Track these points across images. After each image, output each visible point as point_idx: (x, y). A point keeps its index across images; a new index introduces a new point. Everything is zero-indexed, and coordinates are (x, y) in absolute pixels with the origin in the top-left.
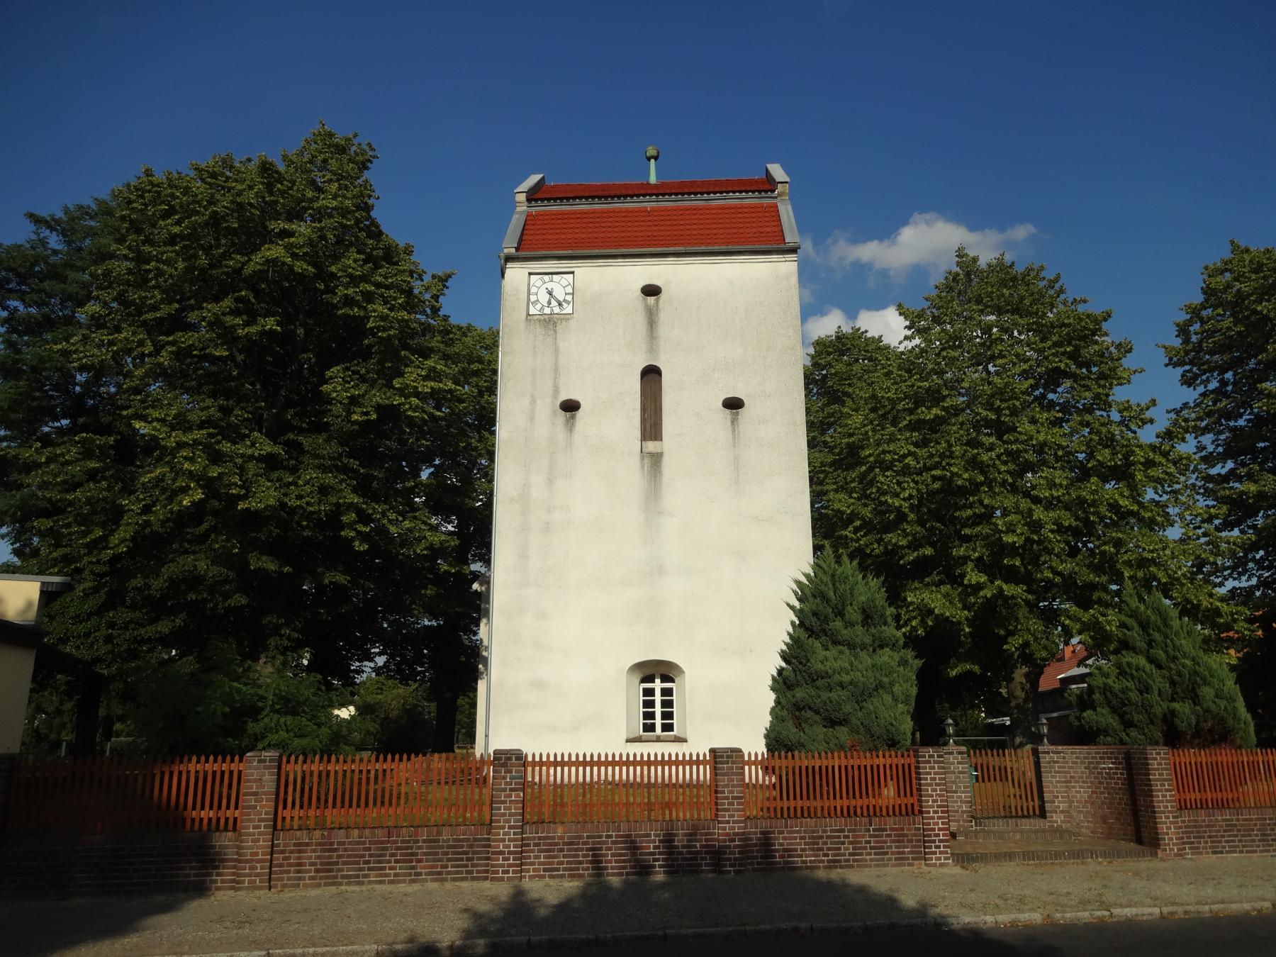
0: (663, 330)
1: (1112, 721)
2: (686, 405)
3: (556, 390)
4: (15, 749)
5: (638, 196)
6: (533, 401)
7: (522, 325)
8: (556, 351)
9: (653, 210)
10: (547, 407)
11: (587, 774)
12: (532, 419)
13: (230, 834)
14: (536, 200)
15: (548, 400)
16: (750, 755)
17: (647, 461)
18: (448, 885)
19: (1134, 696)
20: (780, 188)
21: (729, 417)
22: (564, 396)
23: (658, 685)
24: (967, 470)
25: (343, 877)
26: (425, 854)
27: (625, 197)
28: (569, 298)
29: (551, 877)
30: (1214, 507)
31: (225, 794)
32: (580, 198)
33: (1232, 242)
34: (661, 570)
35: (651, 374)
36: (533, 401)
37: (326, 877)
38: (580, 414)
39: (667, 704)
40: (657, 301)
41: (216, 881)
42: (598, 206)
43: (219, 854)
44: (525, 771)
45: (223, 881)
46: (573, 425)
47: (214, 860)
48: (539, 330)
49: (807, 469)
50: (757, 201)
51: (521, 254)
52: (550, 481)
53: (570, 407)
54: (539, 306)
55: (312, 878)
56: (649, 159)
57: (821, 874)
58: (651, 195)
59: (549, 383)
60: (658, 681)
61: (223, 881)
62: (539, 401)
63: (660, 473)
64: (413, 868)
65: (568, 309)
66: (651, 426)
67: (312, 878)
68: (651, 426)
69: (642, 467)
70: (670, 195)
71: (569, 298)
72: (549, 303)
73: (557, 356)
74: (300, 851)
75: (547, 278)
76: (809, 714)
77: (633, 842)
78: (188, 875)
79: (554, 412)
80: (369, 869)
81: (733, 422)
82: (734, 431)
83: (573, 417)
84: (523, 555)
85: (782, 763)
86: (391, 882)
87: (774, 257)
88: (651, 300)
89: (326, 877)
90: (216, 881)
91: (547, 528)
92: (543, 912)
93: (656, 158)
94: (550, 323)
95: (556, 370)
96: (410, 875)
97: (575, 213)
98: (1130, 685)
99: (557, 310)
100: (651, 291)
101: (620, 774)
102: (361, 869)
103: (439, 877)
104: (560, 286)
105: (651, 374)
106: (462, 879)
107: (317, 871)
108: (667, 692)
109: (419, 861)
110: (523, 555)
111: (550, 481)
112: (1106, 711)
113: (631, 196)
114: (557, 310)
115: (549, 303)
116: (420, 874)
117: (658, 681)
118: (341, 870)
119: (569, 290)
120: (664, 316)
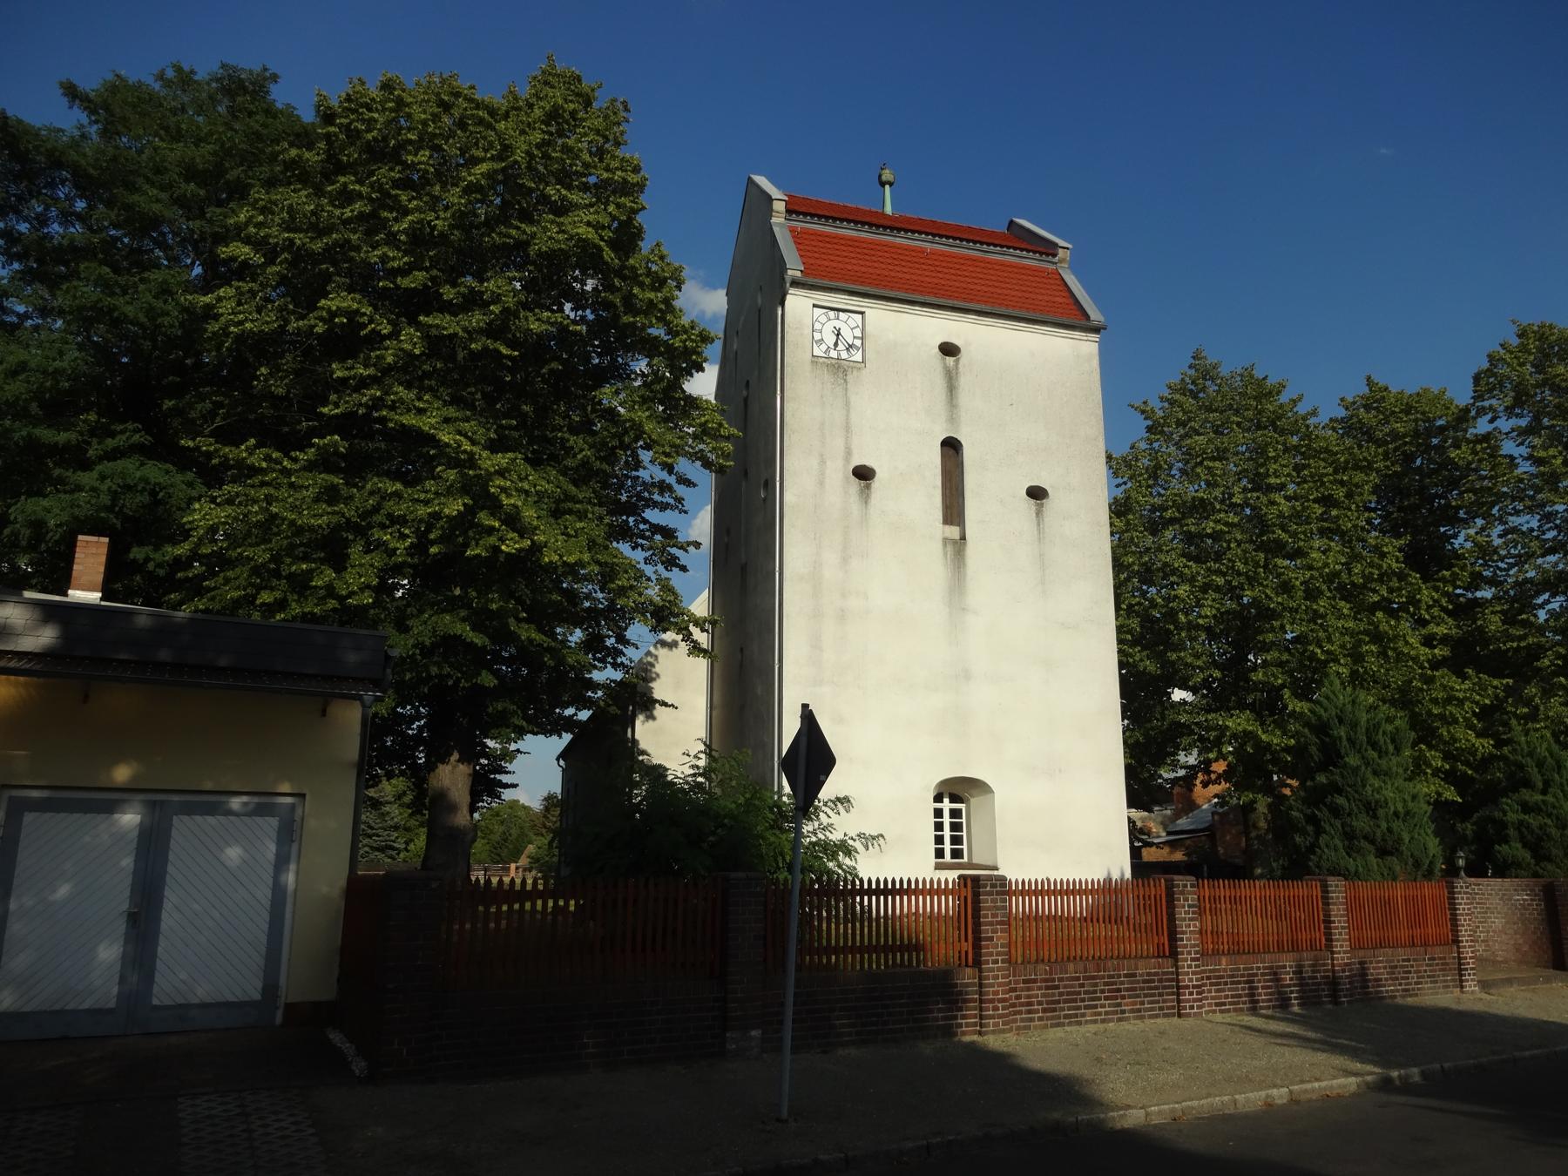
0: (964, 398)
1: (1526, 855)
3: (848, 453)
5: (913, 232)
6: (823, 462)
7: (808, 367)
8: (847, 404)
9: (933, 253)
10: (838, 474)
12: (821, 483)
13: (968, 970)
14: (798, 213)
15: (840, 463)
16: (870, 881)
17: (949, 548)
18: (1148, 1021)
19: (1553, 831)
22: (856, 462)
23: (946, 805)
24: (1277, 594)
25: (1066, 1017)
26: (1127, 990)
27: (899, 230)
28: (858, 343)
29: (1222, 1012)
32: (849, 221)
33: (1369, 378)
34: (967, 675)
35: (951, 447)
36: (823, 462)
38: (876, 483)
39: (956, 827)
40: (957, 362)
41: (960, 1025)
42: (864, 234)
43: (960, 993)
45: (967, 1025)
46: (868, 496)
47: (957, 1001)
48: (827, 377)
50: (863, 235)
51: (810, 280)
52: (845, 560)
53: (864, 474)
54: (824, 347)
55: (1040, 1019)
56: (883, 184)
57: (1399, 1001)
58: (927, 234)
59: (839, 443)
60: (946, 800)
61: (967, 1025)
64: (1119, 1005)
65: (858, 357)
66: (953, 510)
67: (1040, 1019)
68: (953, 510)
70: (948, 237)
71: (858, 343)
72: (836, 344)
74: (1029, 989)
75: (832, 314)
76: (1364, 844)
77: (1275, 974)
78: (937, 1019)
79: (847, 478)
80: (1086, 1007)
83: (868, 487)
84: (816, 644)
86: (1103, 1021)
87: (1077, 334)
88: (950, 360)
89: (1052, 1018)
90: (960, 1025)
91: (842, 616)
93: (891, 184)
94: (839, 369)
95: (847, 428)
96: (1116, 1013)
97: (836, 237)
98: (1549, 822)
99: (844, 355)
100: (948, 350)
102: (1079, 1008)
103: (1139, 1014)
104: (849, 326)
105: (951, 447)
106: (1157, 1016)
107: (1044, 1011)
108: (955, 813)
109: (1123, 997)
110: (816, 644)
111: (845, 560)
112: (1519, 845)
113: (906, 231)
114: (844, 355)
115: (836, 344)
116: (1123, 1012)
117: (946, 800)
118: (1063, 1009)
119: (858, 333)
120: (964, 381)
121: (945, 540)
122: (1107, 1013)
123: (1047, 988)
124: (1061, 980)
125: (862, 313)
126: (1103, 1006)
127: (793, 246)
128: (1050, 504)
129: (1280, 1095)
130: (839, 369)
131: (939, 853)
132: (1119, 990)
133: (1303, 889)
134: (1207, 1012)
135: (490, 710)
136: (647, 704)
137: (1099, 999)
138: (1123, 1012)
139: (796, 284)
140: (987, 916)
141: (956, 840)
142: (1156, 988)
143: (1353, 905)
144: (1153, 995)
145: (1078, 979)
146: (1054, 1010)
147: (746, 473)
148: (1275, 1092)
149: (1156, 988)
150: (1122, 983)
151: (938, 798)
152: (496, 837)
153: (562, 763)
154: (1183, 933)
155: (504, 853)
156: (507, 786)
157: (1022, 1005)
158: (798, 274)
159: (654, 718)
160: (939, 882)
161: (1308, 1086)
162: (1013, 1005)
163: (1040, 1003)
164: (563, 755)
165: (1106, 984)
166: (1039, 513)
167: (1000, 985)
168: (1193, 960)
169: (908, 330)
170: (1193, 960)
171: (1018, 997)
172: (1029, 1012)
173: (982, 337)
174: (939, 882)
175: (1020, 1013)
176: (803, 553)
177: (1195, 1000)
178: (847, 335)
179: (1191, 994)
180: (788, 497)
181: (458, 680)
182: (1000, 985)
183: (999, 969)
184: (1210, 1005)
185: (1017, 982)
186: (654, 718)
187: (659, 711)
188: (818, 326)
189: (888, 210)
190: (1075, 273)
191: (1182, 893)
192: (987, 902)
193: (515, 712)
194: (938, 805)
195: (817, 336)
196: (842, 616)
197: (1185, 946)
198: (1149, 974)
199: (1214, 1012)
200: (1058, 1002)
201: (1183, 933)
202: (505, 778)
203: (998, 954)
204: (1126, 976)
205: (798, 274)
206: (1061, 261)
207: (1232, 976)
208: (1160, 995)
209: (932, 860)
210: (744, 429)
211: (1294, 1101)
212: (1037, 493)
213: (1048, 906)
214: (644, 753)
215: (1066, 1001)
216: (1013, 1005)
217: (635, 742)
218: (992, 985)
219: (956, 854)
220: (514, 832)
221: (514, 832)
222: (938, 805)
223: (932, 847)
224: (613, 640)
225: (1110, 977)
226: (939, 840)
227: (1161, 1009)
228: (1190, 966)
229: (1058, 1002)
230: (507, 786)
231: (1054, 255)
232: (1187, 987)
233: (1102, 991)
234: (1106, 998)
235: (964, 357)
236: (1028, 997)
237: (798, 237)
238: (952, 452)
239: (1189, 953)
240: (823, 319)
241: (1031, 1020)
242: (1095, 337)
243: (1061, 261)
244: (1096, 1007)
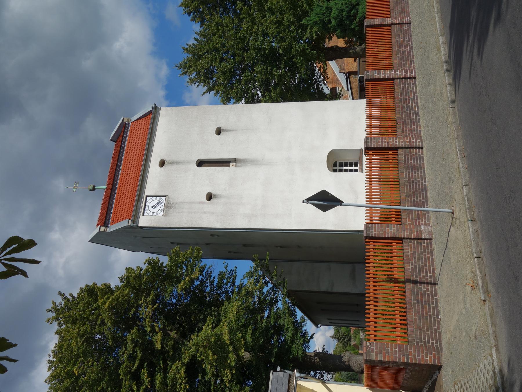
2: (218, 150)
3: (202, 203)
4: (361, 228)
6: (205, 212)
11: (375, 184)
12: (213, 213)
17: (239, 165)
20: (125, 121)
21: (224, 133)
22: (204, 199)
23: (338, 168)
29: (414, 63)
35: (201, 163)
36: (205, 212)
37: (417, 122)
38: (213, 192)
44: (374, 137)
53: (210, 197)
64: (412, 99)
73: (185, 202)
74: (406, 131)
75: (147, 208)
80: (413, 110)
81: (227, 131)
83: (215, 195)
85: (369, 94)
89: (417, 122)
94: (168, 206)
95: (191, 203)
100: (162, 164)
101: (375, 176)
102: (413, 113)
104: (151, 202)
105: (201, 163)
107: (414, 125)
109: (409, 97)
116: (414, 97)
118: (413, 119)
120: (174, 158)
122: (415, 103)
123: (406, 124)
124: (402, 119)
125: (147, 196)
126: (412, 104)
127: (119, 223)
128: (223, 126)
129: (441, 39)
131: (356, 171)
132: (406, 99)
133: (369, 34)
134: (414, 68)
137: (409, 106)
138: (414, 97)
140: (379, 145)
141: (351, 165)
142: (405, 86)
143: (375, 16)
144: (408, 87)
145: (402, 113)
146: (414, 122)
148: (441, 41)
149: (405, 86)
150: (404, 98)
151: (335, 171)
153: (319, 325)
154: (385, 76)
157: (412, 133)
158: (130, 221)
160: (366, 170)
161: (439, 29)
162: (412, 136)
163: (411, 127)
164: (316, 325)
165: (404, 103)
166: (226, 131)
167: (405, 141)
168: (395, 72)
169: (155, 179)
170: (395, 72)
171: (409, 134)
172: (414, 130)
173: (158, 151)
174: (366, 170)
175: (415, 134)
177: (410, 72)
179: (407, 73)
182: (405, 141)
183: (399, 141)
184: (411, 67)
185: (404, 135)
188: (151, 214)
189: (105, 187)
190: (133, 116)
191: (371, 76)
192: (374, 145)
194: (338, 170)
195: (155, 214)
197: (390, 75)
198: (400, 88)
199: (414, 66)
200: (411, 120)
201: (385, 76)
203: (393, 141)
204: (401, 96)
205: (130, 221)
206: (128, 121)
207: (401, 59)
208: (408, 84)
209: (358, 173)
210: (189, 244)
211: (438, 13)
212: (219, 132)
213: (376, 123)
215: (410, 117)
216: (412, 136)
218: (405, 143)
219: (356, 164)
222: (338, 170)
223: (353, 173)
225: (401, 102)
226: (351, 171)
227: (413, 84)
228: (397, 74)
229: (411, 120)
232: (405, 75)
233: (407, 105)
234: (409, 103)
235: (165, 158)
236: (409, 131)
237: (114, 222)
239: (393, 74)
240: (148, 212)
241: (417, 130)
244: (412, 107)
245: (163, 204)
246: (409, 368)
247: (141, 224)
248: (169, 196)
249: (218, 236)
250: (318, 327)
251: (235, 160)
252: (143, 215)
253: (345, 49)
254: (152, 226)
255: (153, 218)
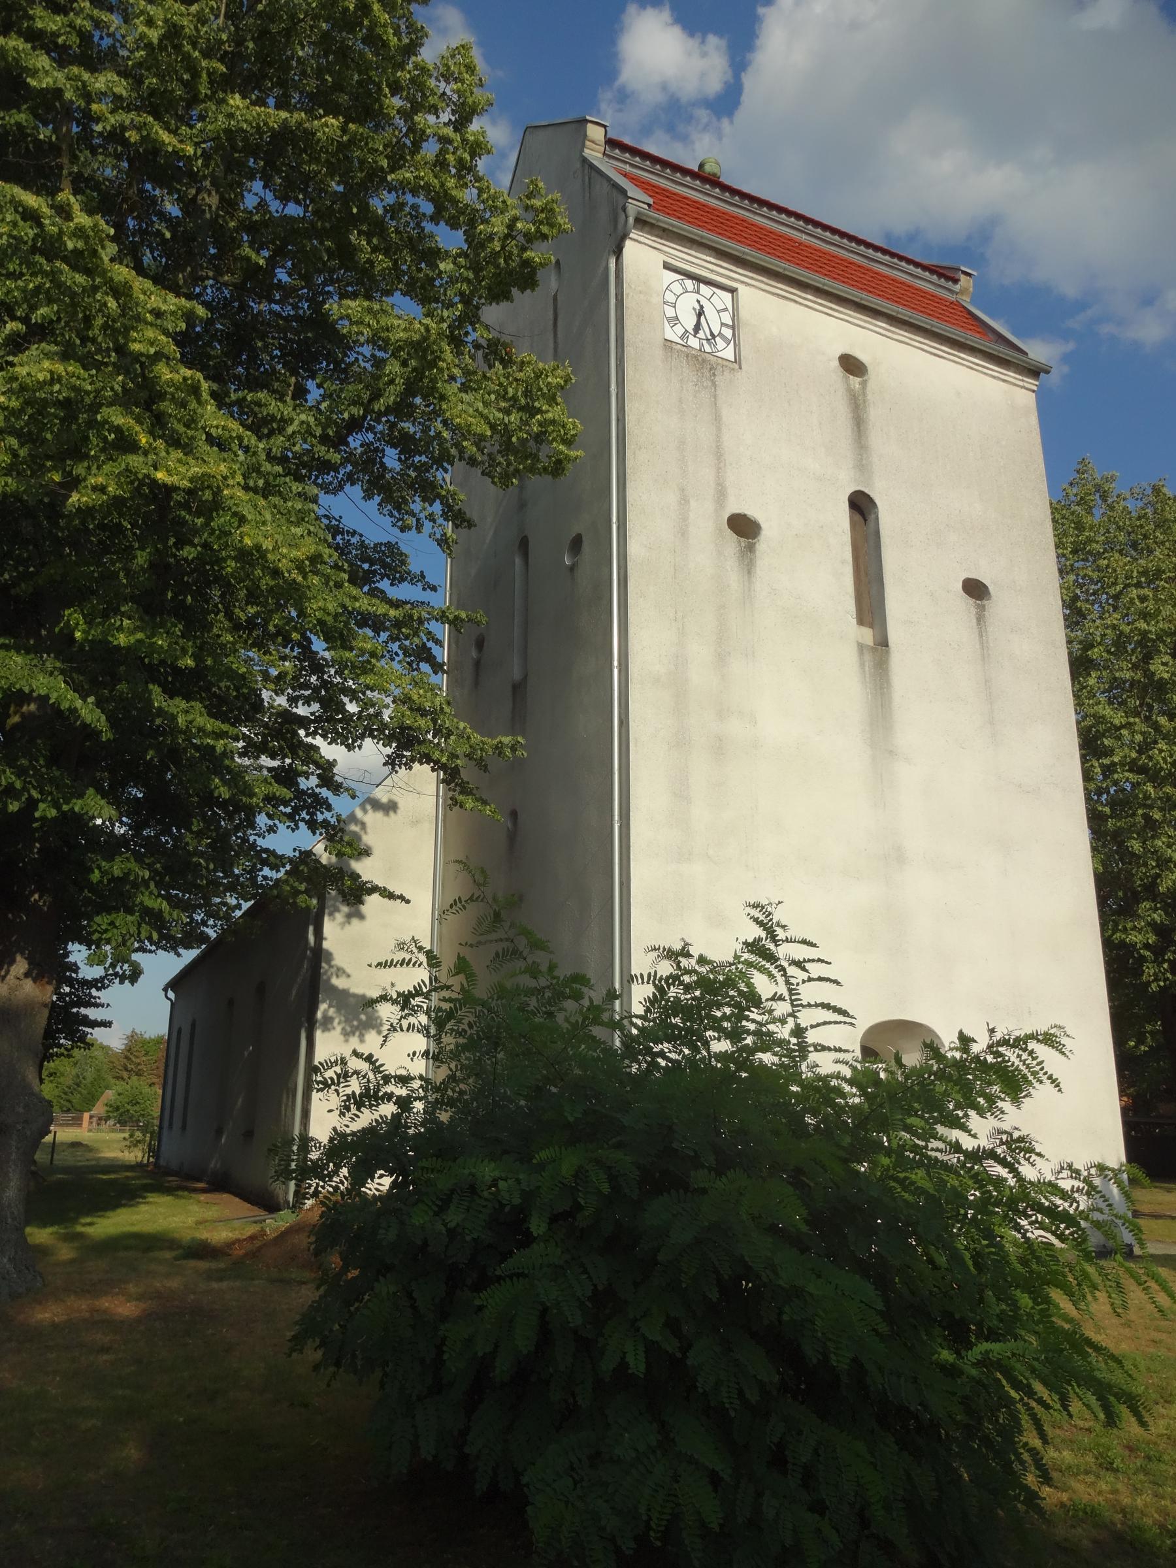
0: (876, 439)
3: (721, 494)
6: (684, 501)
7: (659, 353)
8: (717, 419)
10: (706, 524)
15: (709, 506)
17: (868, 657)
21: (973, 610)
28: (728, 333)
30: (312, 67)
31: (171, 1068)
35: (861, 506)
36: (684, 501)
40: (864, 384)
49: (1073, 718)
52: (721, 660)
53: (743, 527)
54: (679, 330)
62: (693, 503)
63: (888, 682)
69: (862, 665)
72: (697, 327)
73: (719, 429)
75: (689, 284)
82: (981, 636)
83: (751, 548)
87: (1011, 375)
88: (855, 381)
92: (632, 9)
95: (719, 454)
100: (851, 365)
105: (861, 506)
110: (681, 792)
111: (721, 660)
119: (727, 318)
120: (875, 414)
121: (861, 647)
125: (732, 291)
130: (704, 366)
135: (96, 876)
136: (355, 893)
139: (642, 223)
147: (524, 545)
152: (68, 1081)
153: (171, 995)
155: (76, 1099)
156: (95, 1024)
159: (361, 917)
164: (175, 984)
166: (980, 619)
176: (661, 634)
178: (713, 320)
180: (633, 548)
181: (32, 804)
186: (361, 917)
187: (372, 902)
193: (146, 883)
196: (719, 748)
202: (92, 1013)
212: (975, 589)
214: (340, 972)
217: (319, 955)
220: (90, 1075)
221: (90, 1075)
224: (314, 781)
230: (95, 1024)
231: (956, 281)
238: (858, 517)
240: (677, 289)
242: (1032, 383)
243: (962, 292)
245: (707, 348)
246: (315, 901)
247: (631, 249)
248: (739, 375)
249: (572, 569)
250: (165, 990)
251: (881, 646)
252: (667, 266)
253: (28, 1223)
254: (628, 302)
255: (656, 300)
